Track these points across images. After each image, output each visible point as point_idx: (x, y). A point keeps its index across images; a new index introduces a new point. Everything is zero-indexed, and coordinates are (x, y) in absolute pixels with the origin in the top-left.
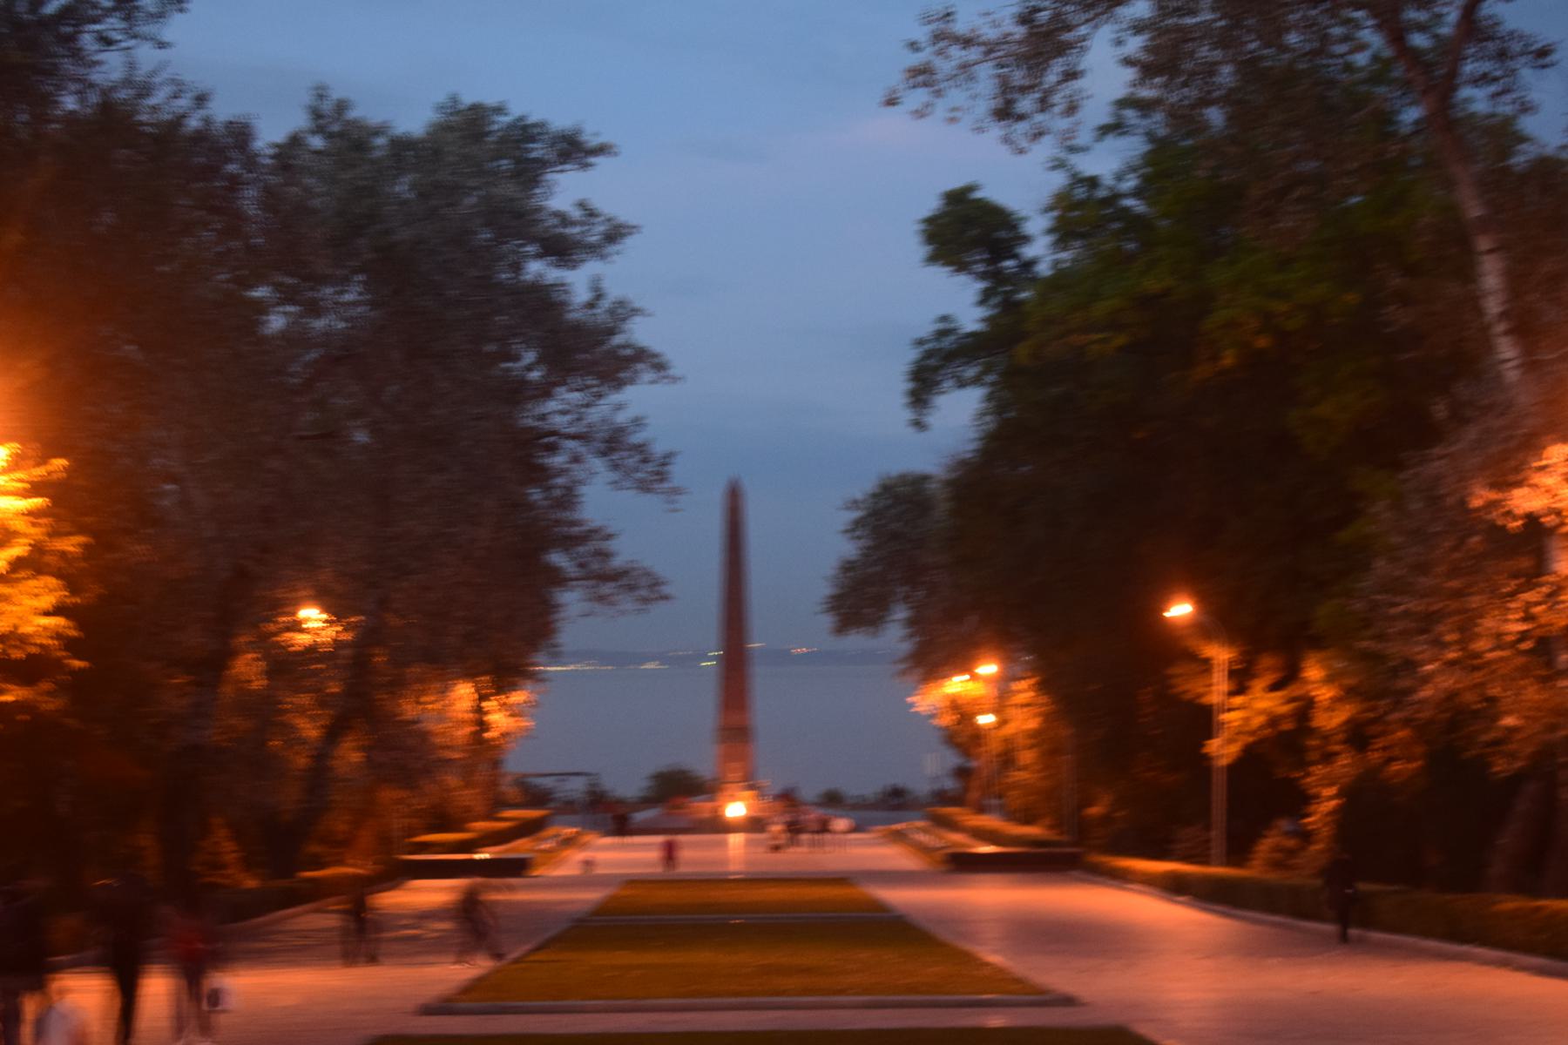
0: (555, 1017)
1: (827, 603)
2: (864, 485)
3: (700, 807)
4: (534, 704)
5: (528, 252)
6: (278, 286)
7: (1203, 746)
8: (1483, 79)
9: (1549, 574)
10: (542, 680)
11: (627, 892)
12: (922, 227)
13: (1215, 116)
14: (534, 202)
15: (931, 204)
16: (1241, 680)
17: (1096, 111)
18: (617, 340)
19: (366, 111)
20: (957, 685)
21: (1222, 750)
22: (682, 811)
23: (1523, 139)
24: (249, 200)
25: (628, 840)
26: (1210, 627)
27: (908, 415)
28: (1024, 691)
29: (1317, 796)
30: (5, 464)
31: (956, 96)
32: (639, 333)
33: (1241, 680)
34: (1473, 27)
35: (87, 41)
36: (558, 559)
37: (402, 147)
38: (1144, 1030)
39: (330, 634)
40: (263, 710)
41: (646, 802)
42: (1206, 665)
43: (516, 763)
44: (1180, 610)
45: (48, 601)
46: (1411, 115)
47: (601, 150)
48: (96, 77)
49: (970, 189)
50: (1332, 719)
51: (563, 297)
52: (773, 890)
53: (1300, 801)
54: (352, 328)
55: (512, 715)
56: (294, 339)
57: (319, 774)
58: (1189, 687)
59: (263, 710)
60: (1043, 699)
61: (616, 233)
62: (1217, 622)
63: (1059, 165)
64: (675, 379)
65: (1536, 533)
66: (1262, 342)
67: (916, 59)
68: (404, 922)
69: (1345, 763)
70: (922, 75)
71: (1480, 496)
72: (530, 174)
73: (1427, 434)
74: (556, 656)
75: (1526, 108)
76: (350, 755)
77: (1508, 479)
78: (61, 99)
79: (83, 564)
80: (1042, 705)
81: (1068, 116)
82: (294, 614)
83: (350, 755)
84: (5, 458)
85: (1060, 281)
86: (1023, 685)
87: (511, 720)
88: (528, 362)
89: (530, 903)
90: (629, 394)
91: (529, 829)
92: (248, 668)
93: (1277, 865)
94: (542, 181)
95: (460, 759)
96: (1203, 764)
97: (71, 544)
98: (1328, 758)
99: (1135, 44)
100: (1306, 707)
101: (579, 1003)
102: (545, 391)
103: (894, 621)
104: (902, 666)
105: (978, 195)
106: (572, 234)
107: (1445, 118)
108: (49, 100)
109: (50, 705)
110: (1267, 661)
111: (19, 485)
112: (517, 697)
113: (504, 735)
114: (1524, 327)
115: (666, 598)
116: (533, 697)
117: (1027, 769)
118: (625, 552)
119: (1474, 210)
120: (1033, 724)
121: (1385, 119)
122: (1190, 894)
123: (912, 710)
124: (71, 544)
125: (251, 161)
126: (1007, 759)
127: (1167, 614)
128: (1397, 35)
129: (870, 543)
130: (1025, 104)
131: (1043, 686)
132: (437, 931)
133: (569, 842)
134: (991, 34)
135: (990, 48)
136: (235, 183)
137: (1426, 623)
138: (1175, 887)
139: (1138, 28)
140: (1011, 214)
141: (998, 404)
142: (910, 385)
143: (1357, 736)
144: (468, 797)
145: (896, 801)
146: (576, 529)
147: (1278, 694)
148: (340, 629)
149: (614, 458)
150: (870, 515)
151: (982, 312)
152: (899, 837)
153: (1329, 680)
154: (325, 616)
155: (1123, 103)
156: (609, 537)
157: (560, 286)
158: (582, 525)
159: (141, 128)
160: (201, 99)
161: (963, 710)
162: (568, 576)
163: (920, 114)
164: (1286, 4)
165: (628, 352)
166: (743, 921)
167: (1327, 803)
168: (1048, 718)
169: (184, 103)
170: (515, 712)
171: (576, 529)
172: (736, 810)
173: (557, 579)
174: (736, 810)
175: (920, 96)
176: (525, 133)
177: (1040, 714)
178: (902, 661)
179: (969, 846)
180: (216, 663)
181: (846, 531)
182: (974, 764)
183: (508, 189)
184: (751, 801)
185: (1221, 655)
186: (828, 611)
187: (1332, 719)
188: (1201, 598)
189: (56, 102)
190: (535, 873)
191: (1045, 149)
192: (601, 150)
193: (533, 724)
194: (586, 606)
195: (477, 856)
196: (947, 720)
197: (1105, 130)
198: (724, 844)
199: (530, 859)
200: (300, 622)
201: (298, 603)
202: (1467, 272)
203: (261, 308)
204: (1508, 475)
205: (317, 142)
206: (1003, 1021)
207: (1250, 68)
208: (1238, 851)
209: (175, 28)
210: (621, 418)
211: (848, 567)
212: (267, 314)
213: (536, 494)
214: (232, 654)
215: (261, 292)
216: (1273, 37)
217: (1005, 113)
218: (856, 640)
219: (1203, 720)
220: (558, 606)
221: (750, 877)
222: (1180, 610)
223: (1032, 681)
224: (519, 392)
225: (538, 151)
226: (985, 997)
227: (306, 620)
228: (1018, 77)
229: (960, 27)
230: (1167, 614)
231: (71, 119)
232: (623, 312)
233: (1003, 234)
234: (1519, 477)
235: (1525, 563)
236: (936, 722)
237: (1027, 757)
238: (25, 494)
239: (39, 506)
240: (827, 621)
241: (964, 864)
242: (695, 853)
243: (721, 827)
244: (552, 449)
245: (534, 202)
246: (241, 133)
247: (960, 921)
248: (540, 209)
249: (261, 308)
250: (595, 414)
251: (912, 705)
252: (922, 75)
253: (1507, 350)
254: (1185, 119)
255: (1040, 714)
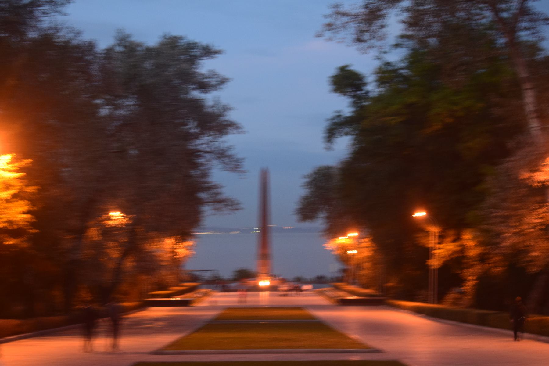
0: (284, 355)
1: (298, 211)
2: (309, 169)
3: (251, 282)
4: (196, 246)
5: (190, 88)
6: (106, 99)
7: (426, 262)
8: (526, 29)
9: (547, 202)
10: (197, 238)
11: (227, 312)
12: (330, 79)
13: (433, 41)
14: (193, 70)
15: (333, 72)
16: (442, 238)
17: (391, 40)
18: (222, 119)
19: (136, 38)
20: (342, 240)
21: (434, 263)
22: (245, 284)
23: (541, 50)
24: (94, 69)
25: (227, 294)
26: (431, 220)
27: (324, 145)
28: (366, 242)
29: (466, 280)
30: (10, 161)
31: (342, 34)
32: (231, 116)
33: (442, 238)
34: (524, 11)
35: (37, 13)
36: (203, 195)
37: (149, 50)
38: (406, 361)
39: (124, 221)
40: (98, 247)
41: (235, 280)
42: (427, 233)
43: (189, 267)
44: (420, 214)
45: (26, 208)
46: (502, 41)
47: (216, 52)
48: (39, 25)
49: (347, 66)
50: (473, 253)
51: (203, 104)
52: (275, 312)
53: (460, 281)
54: (132, 113)
55: (188, 250)
56: (110, 118)
57: (118, 271)
58: (424, 241)
59: (98, 247)
60: (374, 245)
61: (223, 81)
62: (434, 218)
63: (378, 58)
64: (244, 132)
65: (543, 188)
66: (450, 120)
67: (329, 20)
68: (147, 322)
69: (477, 269)
70: (330, 26)
71: (525, 175)
72: (193, 60)
73: (506, 153)
74: (204, 230)
75: (543, 39)
76: (129, 264)
77: (535, 169)
78: (27, 33)
79: (37, 196)
80: (373, 247)
81: (401, 38)
82: (108, 214)
83: (129, 264)
84: (11, 159)
85: (378, 100)
86: (366, 240)
87: (187, 251)
88: (192, 127)
89: (197, 316)
90: (225, 138)
91: (192, 290)
92: (93, 233)
93: (454, 304)
94: (195, 63)
95: (168, 265)
96: (426, 269)
97: (31, 189)
98: (472, 266)
99: (405, 16)
100: (463, 249)
101: (183, 351)
102: (196, 136)
103: (319, 218)
104: (321, 233)
105: (348, 68)
106: (207, 81)
107: (514, 43)
108: (23, 34)
109: (25, 245)
110: (452, 232)
111: (14, 168)
112: (190, 243)
113: (185, 257)
114: (541, 115)
115: (242, 209)
116: (195, 243)
117: (366, 272)
118: (226, 192)
119: (523, 74)
120: (370, 254)
121: (492, 42)
122: (424, 314)
123: (325, 249)
124: (31, 189)
125: (94, 55)
126: (359, 266)
127: (414, 216)
128: (496, 11)
129: (313, 190)
130: (366, 36)
131: (374, 241)
132: (161, 325)
133: (206, 294)
134: (354, 12)
135: (356, 16)
136: (91, 63)
137: (505, 219)
138: (418, 311)
139: (408, 10)
140: (360, 75)
141: (358, 141)
142: (327, 135)
143: (482, 258)
144: (170, 278)
145: (320, 281)
146: (206, 185)
147: (454, 244)
148: (127, 219)
149: (224, 159)
150: (313, 180)
151: (353, 109)
152: (321, 293)
153: (473, 239)
154: (122, 215)
155: (402, 37)
156: (221, 187)
157: (202, 100)
158: (210, 183)
159: (55, 44)
160: (78, 33)
161: (345, 248)
162: (205, 201)
163: (330, 39)
164: (459, 2)
165: (225, 123)
166: (268, 322)
167: (470, 284)
168: (375, 251)
169: (71, 35)
170: (188, 248)
171: (206, 185)
172: (264, 283)
173: (202, 202)
174: (264, 283)
175: (328, 34)
176: (191, 46)
177: (373, 250)
178: (321, 232)
179: (345, 297)
180: (81, 232)
181: (301, 186)
182: (349, 267)
183: (184, 66)
184: (270, 280)
185: (434, 230)
186: (296, 214)
187: (473, 253)
188: (428, 210)
189: (26, 34)
190: (192, 305)
191: (373, 53)
192: (216, 52)
193: (195, 252)
194: (214, 212)
195: (172, 299)
196: (337, 252)
197: (397, 46)
198: (258, 295)
199: (193, 300)
200: (110, 217)
201: (108, 211)
202: (519, 95)
203: (98, 106)
204: (535, 167)
205: (118, 49)
206: (358, 358)
207: (445, 24)
208: (440, 299)
209: (69, 9)
210: (226, 145)
211: (306, 198)
212: (99, 109)
213: (193, 172)
214: (87, 228)
215: (98, 101)
216: (453, 14)
217: (359, 40)
218: (307, 224)
219: (427, 253)
220: (202, 212)
221: (271, 307)
222: (420, 214)
223: (370, 239)
224: (189, 137)
225: (196, 52)
226: (352, 349)
227: (113, 216)
228: (364, 27)
229: (342, 10)
230: (414, 216)
231: (34, 41)
232: (226, 109)
233: (357, 82)
234: (536, 168)
235: (538, 199)
236: (333, 253)
237: (367, 265)
238: (17, 171)
239: (22, 175)
240: (295, 217)
241: (345, 303)
242: (251, 299)
243: (258, 289)
244: (199, 156)
245: (193, 70)
246: (91, 46)
247: (342, 322)
248: (194, 73)
249: (98, 106)
250: (217, 144)
251: (324, 247)
252: (330, 26)
253: (534, 124)
254: (422, 42)
255: (373, 250)
